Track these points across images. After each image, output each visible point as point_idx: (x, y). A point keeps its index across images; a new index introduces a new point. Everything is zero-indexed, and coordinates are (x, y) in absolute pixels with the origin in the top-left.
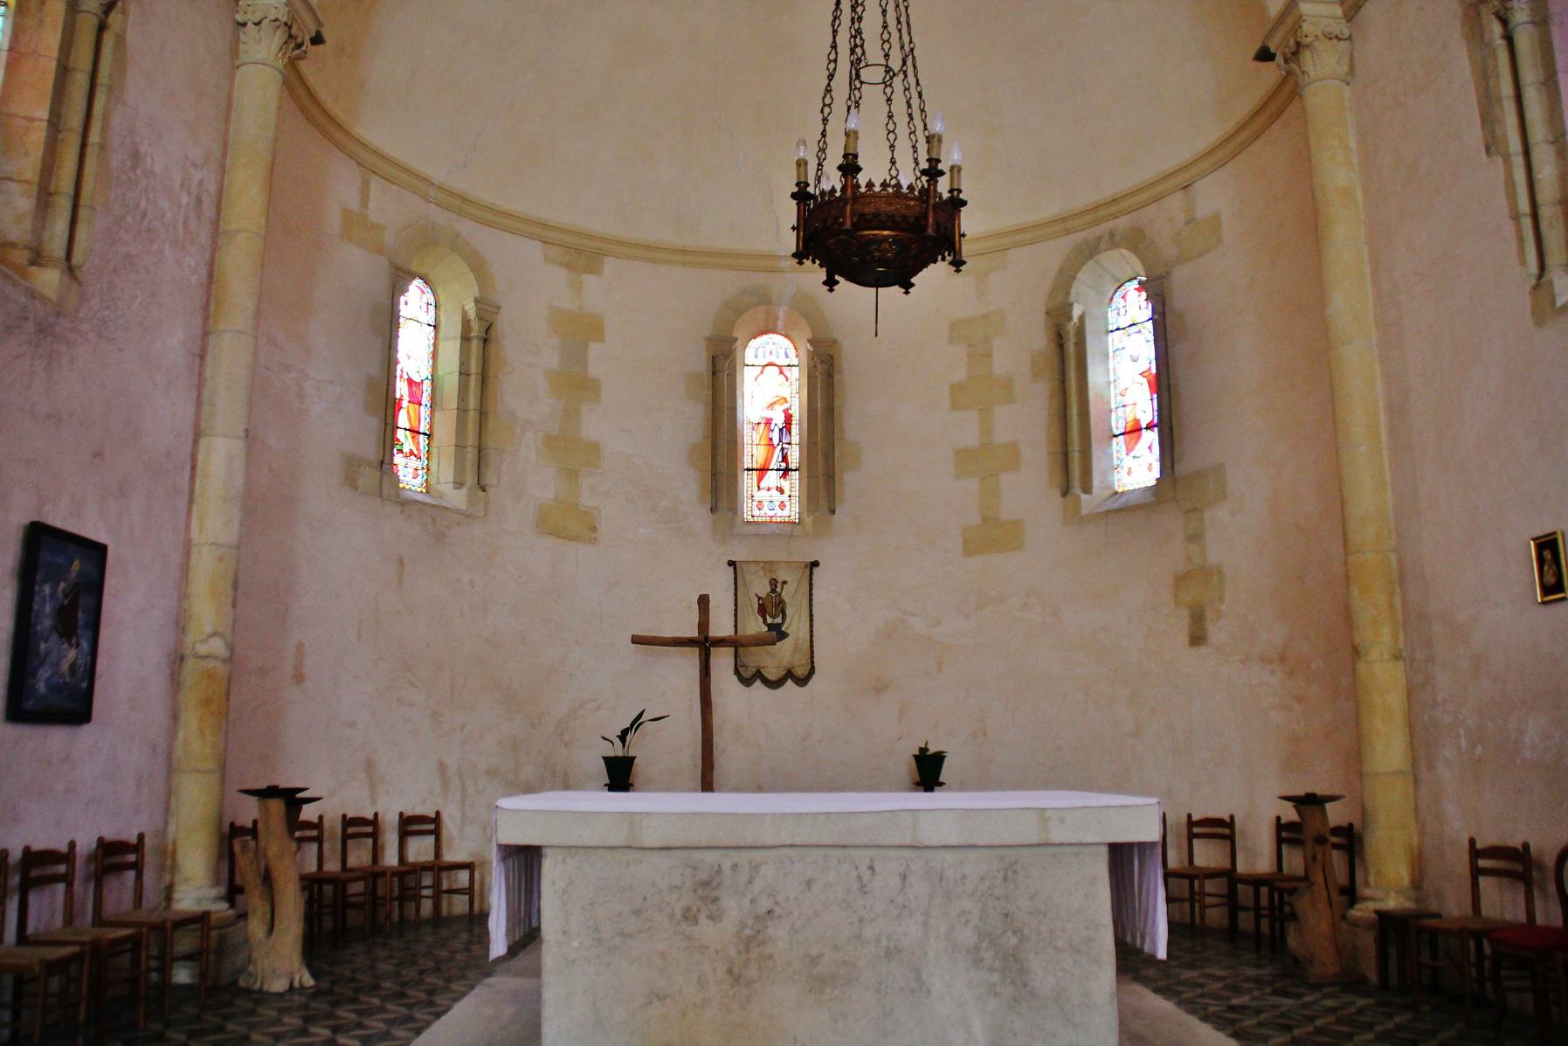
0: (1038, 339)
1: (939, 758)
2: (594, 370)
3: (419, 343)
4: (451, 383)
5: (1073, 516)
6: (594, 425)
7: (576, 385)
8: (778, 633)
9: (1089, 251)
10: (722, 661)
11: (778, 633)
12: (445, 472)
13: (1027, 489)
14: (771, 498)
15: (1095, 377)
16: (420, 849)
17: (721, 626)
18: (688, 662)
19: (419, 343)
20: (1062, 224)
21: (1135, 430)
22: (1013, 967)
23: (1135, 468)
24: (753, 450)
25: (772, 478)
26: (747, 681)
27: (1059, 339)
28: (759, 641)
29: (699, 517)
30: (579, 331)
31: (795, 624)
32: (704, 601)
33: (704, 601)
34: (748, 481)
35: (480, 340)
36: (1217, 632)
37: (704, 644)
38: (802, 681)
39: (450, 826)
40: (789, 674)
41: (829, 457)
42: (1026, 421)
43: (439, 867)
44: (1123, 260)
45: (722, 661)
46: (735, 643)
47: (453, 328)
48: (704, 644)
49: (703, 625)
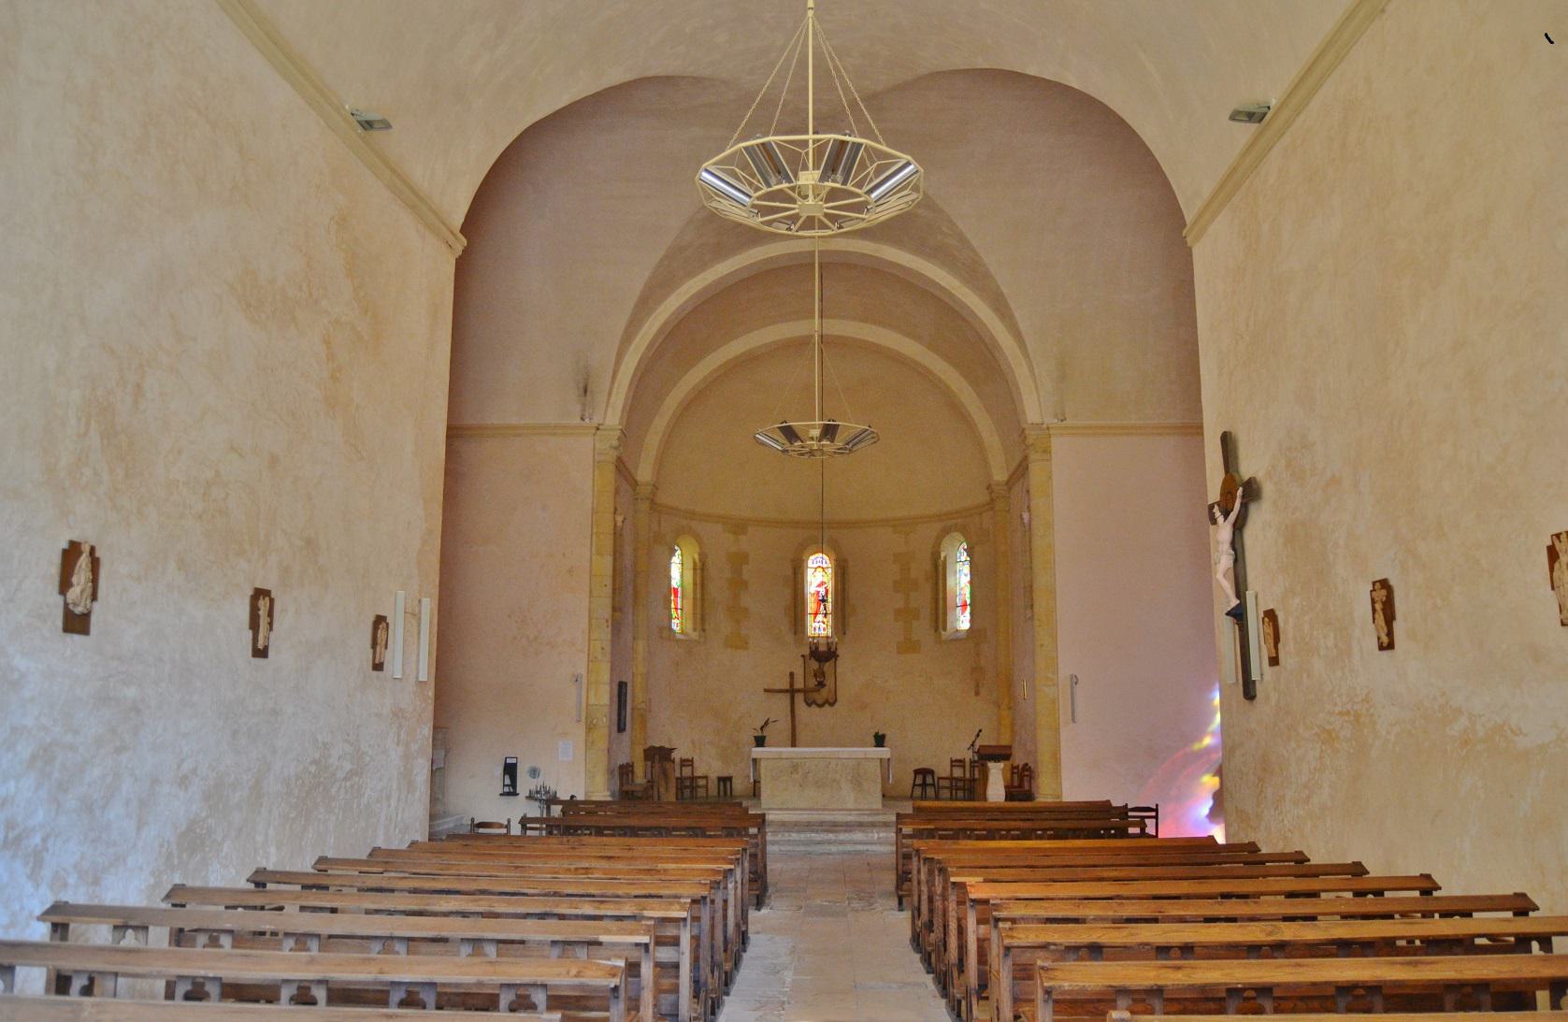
0: (928, 566)
1: (883, 737)
2: (745, 577)
3: (677, 571)
4: (690, 588)
5: (939, 641)
6: (746, 600)
7: (738, 584)
8: (821, 684)
9: (946, 531)
10: (799, 698)
11: (821, 684)
12: (689, 626)
13: (921, 628)
14: (819, 627)
15: (950, 582)
16: (687, 772)
17: (799, 684)
18: (785, 699)
19: (677, 571)
20: (939, 517)
21: (964, 605)
22: (309, 542)
23: (963, 622)
24: (811, 605)
25: (820, 617)
26: (809, 705)
27: (936, 566)
28: (813, 691)
29: (789, 637)
30: (738, 560)
31: (829, 682)
32: (792, 675)
33: (792, 675)
34: (810, 618)
35: (701, 571)
36: (983, 691)
37: (792, 692)
38: (832, 704)
39: (696, 763)
40: (827, 702)
41: (843, 610)
42: (922, 599)
43: (693, 779)
44: (958, 536)
45: (799, 698)
46: (805, 691)
47: (689, 565)
48: (792, 692)
49: (792, 684)
